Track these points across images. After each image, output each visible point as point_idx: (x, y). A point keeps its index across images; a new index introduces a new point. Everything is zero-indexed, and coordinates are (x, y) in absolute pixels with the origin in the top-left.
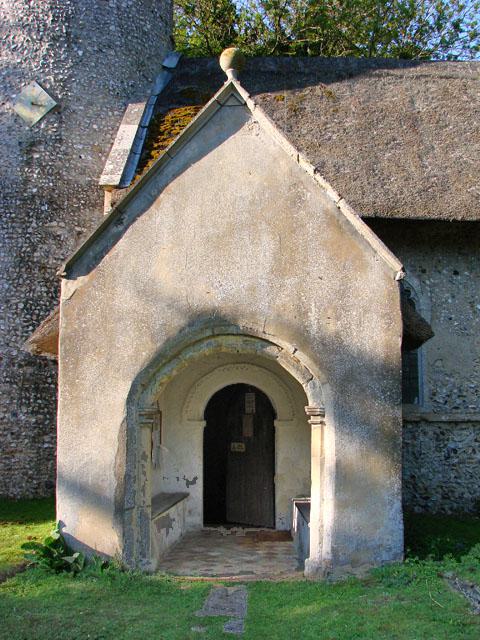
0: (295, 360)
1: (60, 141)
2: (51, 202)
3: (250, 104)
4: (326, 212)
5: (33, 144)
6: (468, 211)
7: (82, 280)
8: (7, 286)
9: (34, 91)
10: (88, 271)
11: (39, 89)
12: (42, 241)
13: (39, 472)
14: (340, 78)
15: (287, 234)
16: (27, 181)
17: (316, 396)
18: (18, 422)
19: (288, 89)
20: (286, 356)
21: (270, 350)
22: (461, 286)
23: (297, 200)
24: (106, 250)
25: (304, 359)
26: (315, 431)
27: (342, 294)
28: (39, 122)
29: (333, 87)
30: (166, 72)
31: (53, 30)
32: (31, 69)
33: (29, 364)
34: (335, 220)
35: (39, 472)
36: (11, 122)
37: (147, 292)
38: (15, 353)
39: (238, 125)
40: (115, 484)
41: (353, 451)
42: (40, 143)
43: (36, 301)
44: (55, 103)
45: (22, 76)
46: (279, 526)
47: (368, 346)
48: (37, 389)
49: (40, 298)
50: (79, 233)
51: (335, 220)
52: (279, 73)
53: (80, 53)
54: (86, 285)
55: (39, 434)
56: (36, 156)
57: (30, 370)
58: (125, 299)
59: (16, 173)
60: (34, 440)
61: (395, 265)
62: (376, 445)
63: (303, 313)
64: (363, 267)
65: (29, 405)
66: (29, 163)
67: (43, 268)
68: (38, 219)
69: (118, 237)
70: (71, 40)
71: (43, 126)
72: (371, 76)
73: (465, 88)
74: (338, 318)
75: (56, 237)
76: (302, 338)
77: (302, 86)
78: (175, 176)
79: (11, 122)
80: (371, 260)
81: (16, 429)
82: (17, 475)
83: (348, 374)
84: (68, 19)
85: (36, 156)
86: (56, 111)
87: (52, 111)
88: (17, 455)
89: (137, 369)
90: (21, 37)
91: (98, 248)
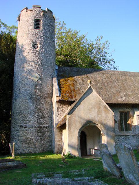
0: (100, 126)
1: (41, 85)
2: (41, 97)
3: (93, 89)
4: (104, 106)
5: (36, 85)
6: (116, 102)
7: (70, 115)
8: (33, 113)
9: (36, 75)
10: (71, 114)
11: (37, 74)
12: (39, 104)
13: (41, 148)
14: (88, 73)
15: (99, 108)
16: (36, 92)
17: (103, 132)
18: (37, 139)
19: (80, 75)
20: (99, 126)
21: (97, 125)
22: (23, 91)
23: (100, 104)
24: (74, 111)
25: (102, 127)
26: (103, 137)
27: (106, 117)
28: (37, 81)
29: (88, 75)
30: (138, 116)
31: (39, 63)
32: (35, 70)
33: (38, 127)
34: (105, 107)
35: (41, 148)
36: (31, 81)
37: (80, 117)
38: (36, 125)
39: (91, 92)
40: (77, 145)
41: (109, 139)
42: (38, 85)
43: (39, 116)
44: (40, 77)
45: (33, 71)
46: (88, 153)
47: (110, 125)
48: (40, 132)
49: (40, 115)
50: (46, 103)
51: (105, 107)
52: (77, 72)
53: (44, 67)
54: (71, 116)
55: (41, 141)
56: (37, 88)
57: (39, 129)
58: (77, 118)
59: (34, 91)
60: (40, 142)
61: (113, 113)
62: (112, 138)
63: (102, 120)
64: (109, 113)
65: (39, 135)
66: (36, 89)
67: (40, 109)
68: (39, 100)
69: (75, 109)
70: (42, 65)
71: (38, 82)
72: (94, 73)
73: (110, 77)
74: (106, 121)
75: (42, 103)
76: (102, 124)
77: (82, 75)
78: (83, 100)
79: (31, 81)
80: (110, 112)
81: (37, 140)
82: (37, 149)
83: (108, 128)
84: (41, 61)
85: (37, 88)
86: (40, 79)
87: (40, 78)
88: (37, 145)
89: (79, 128)
90: (33, 64)
91: (73, 110)
